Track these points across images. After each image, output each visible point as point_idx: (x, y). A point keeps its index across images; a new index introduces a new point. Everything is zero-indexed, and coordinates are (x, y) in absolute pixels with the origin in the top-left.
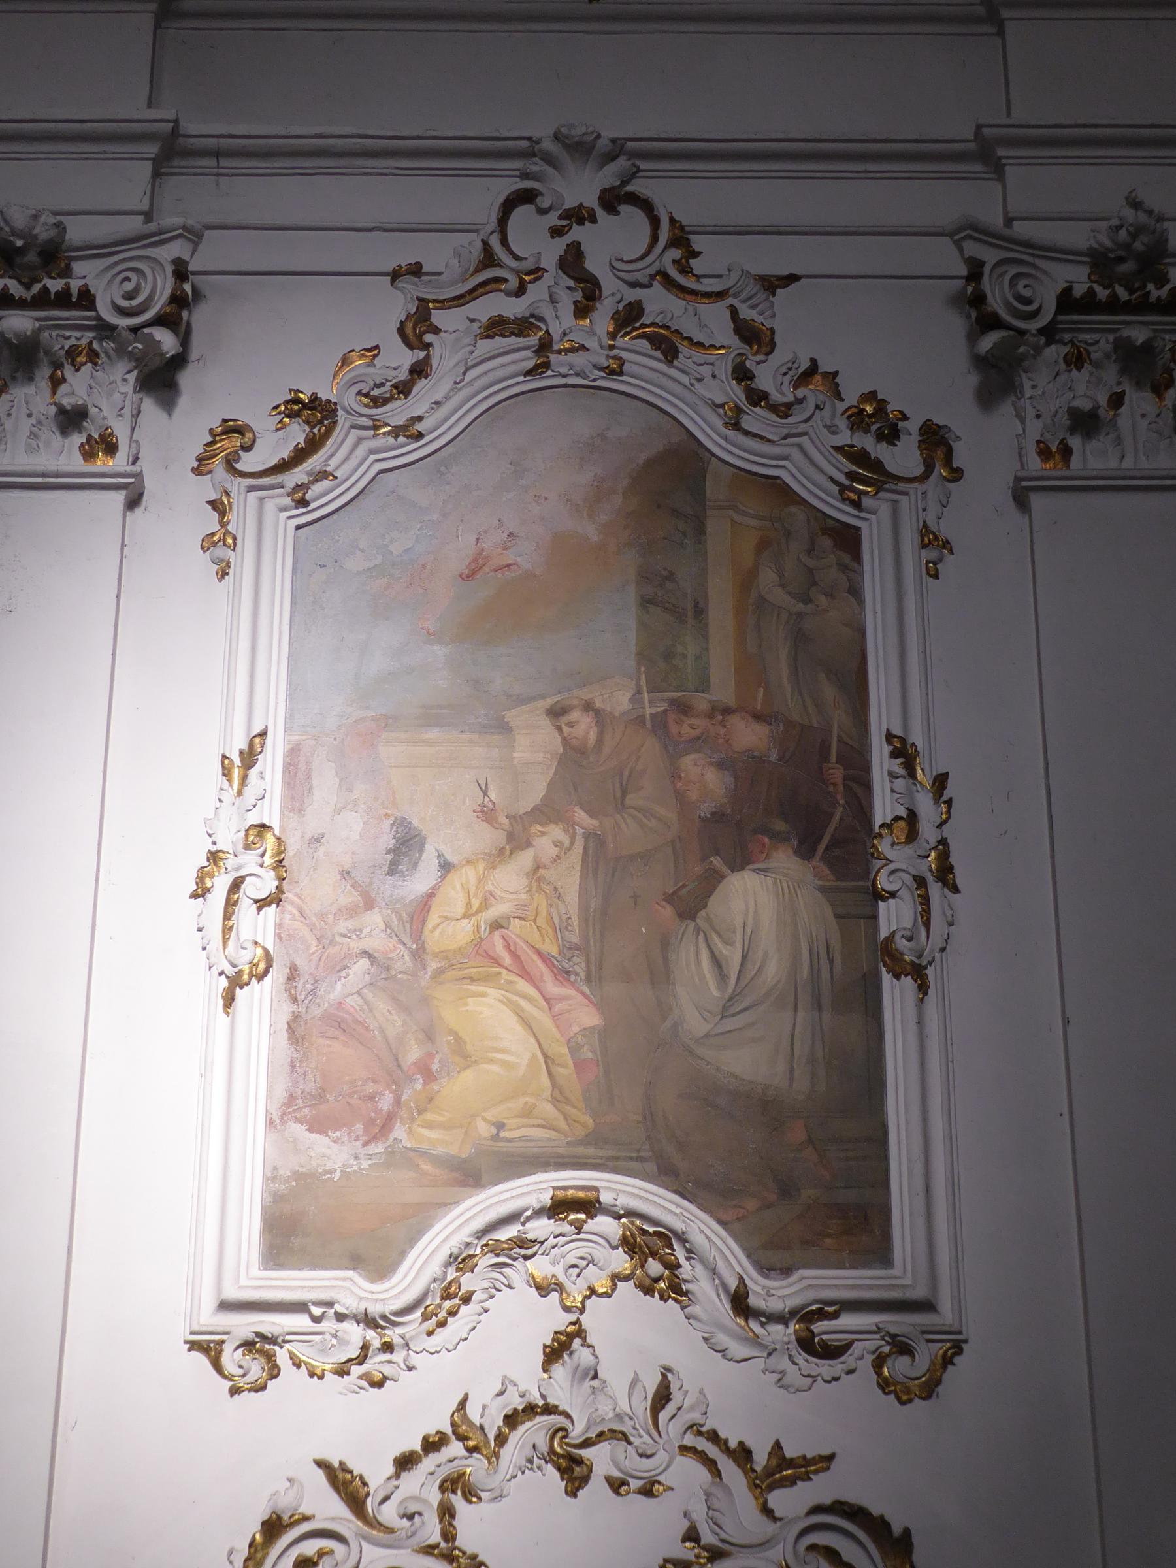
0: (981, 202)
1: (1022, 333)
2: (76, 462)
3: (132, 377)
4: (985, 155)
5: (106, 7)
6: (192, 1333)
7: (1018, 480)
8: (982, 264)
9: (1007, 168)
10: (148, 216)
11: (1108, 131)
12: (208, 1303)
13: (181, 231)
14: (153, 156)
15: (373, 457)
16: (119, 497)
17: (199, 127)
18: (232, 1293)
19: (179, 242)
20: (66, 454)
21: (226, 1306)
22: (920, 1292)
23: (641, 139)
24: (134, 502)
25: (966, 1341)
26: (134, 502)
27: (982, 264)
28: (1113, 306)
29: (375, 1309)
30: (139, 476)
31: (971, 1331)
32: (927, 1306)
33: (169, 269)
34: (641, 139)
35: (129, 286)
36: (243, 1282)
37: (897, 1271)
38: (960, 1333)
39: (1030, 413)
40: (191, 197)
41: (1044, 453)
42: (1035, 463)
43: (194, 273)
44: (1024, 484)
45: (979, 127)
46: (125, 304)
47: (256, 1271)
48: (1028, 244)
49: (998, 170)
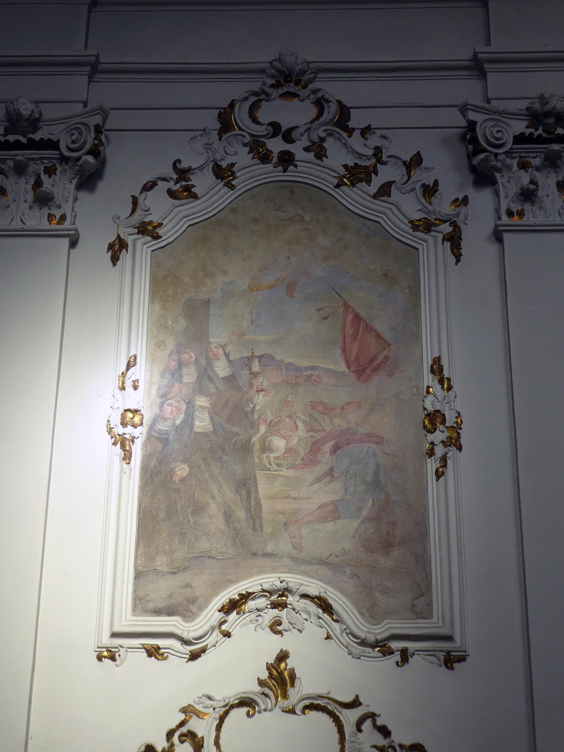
0: (467, 90)
1: (496, 155)
2: (45, 225)
3: (74, 182)
4: (477, 67)
5: (391, 6)
6: (98, 648)
7: (496, 226)
8: (475, 123)
9: (488, 74)
10: (85, 104)
11: (407, 64)
12: (106, 634)
13: (99, 111)
14: (88, 73)
15: (185, 219)
16: (66, 241)
17: (108, 59)
18: (118, 629)
19: (98, 116)
20: (37, 219)
21: (115, 635)
22: (445, 631)
23: (528, 52)
24: (73, 244)
25: (468, 656)
26: (73, 244)
27: (475, 123)
28: (540, 140)
29: (185, 635)
30: (76, 230)
31: (470, 651)
32: (449, 638)
33: (92, 129)
34: (528, 52)
35: (74, 137)
36: (124, 622)
37: (435, 619)
38: (465, 652)
39: (502, 194)
40: (106, 93)
41: (510, 214)
42: (505, 219)
43: (106, 130)
44: (500, 228)
45: (475, 54)
46: (73, 146)
47: (129, 616)
48: (499, 113)
49: (483, 75)
